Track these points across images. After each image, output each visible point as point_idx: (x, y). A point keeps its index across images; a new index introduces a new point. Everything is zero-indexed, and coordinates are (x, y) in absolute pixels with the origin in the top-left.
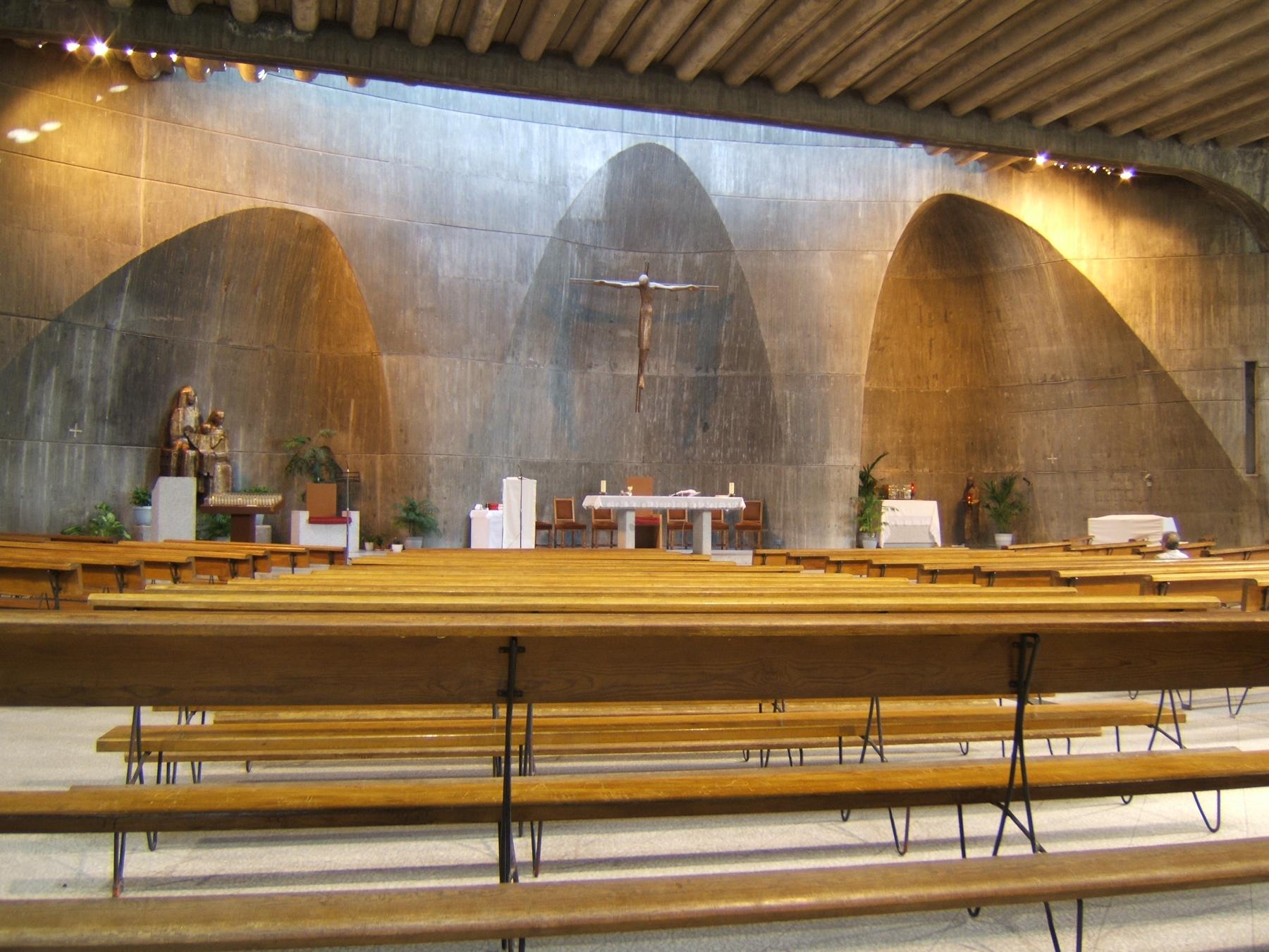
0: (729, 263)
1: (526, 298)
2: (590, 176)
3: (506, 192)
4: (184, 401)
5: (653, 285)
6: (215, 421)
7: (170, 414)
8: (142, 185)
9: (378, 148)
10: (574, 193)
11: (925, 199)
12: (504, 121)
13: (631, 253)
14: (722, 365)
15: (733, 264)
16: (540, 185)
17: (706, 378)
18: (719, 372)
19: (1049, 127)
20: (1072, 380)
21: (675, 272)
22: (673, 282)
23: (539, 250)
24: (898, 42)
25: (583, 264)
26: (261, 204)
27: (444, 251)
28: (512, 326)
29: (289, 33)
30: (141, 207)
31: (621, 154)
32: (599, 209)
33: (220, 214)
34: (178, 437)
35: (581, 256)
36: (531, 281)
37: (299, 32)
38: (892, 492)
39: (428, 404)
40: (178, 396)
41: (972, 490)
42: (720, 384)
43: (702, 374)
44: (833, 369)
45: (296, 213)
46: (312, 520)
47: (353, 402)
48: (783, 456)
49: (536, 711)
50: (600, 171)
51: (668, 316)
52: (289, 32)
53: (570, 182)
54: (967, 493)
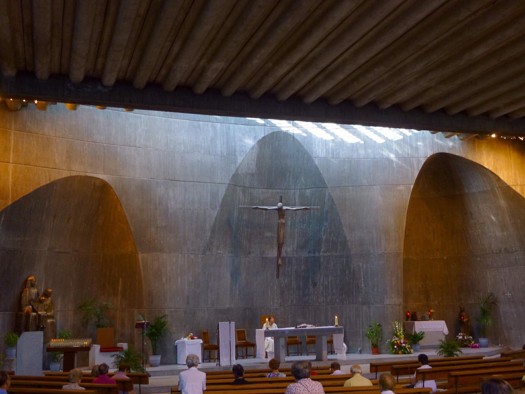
0: (325, 194)
1: (216, 218)
2: (248, 150)
3: (203, 161)
4: (29, 285)
5: (284, 208)
6: (47, 295)
7: (22, 293)
8: (11, 167)
9: (135, 140)
10: (240, 160)
11: (429, 156)
12: (201, 123)
13: (270, 190)
14: (323, 250)
15: (327, 194)
16: (221, 156)
17: (314, 257)
18: (321, 254)
19: (498, 119)
20: (516, 251)
21: (295, 200)
22: (295, 206)
23: (222, 191)
24: (424, 83)
25: (245, 197)
26: (74, 174)
27: (171, 194)
28: (209, 234)
29: (100, 88)
30: (10, 179)
31: (264, 138)
32: (253, 167)
33: (52, 180)
34: (26, 305)
35: (244, 193)
36: (218, 208)
37: (105, 87)
38: (419, 316)
39: (164, 280)
40: (26, 281)
41: (463, 314)
42: (322, 260)
43: (312, 255)
44: (386, 250)
45: (92, 178)
46: (102, 350)
47: (121, 279)
48: (360, 300)
49: (141, 385)
50: (253, 147)
51: (291, 223)
52: (100, 87)
53: (237, 154)
54: (460, 315)
